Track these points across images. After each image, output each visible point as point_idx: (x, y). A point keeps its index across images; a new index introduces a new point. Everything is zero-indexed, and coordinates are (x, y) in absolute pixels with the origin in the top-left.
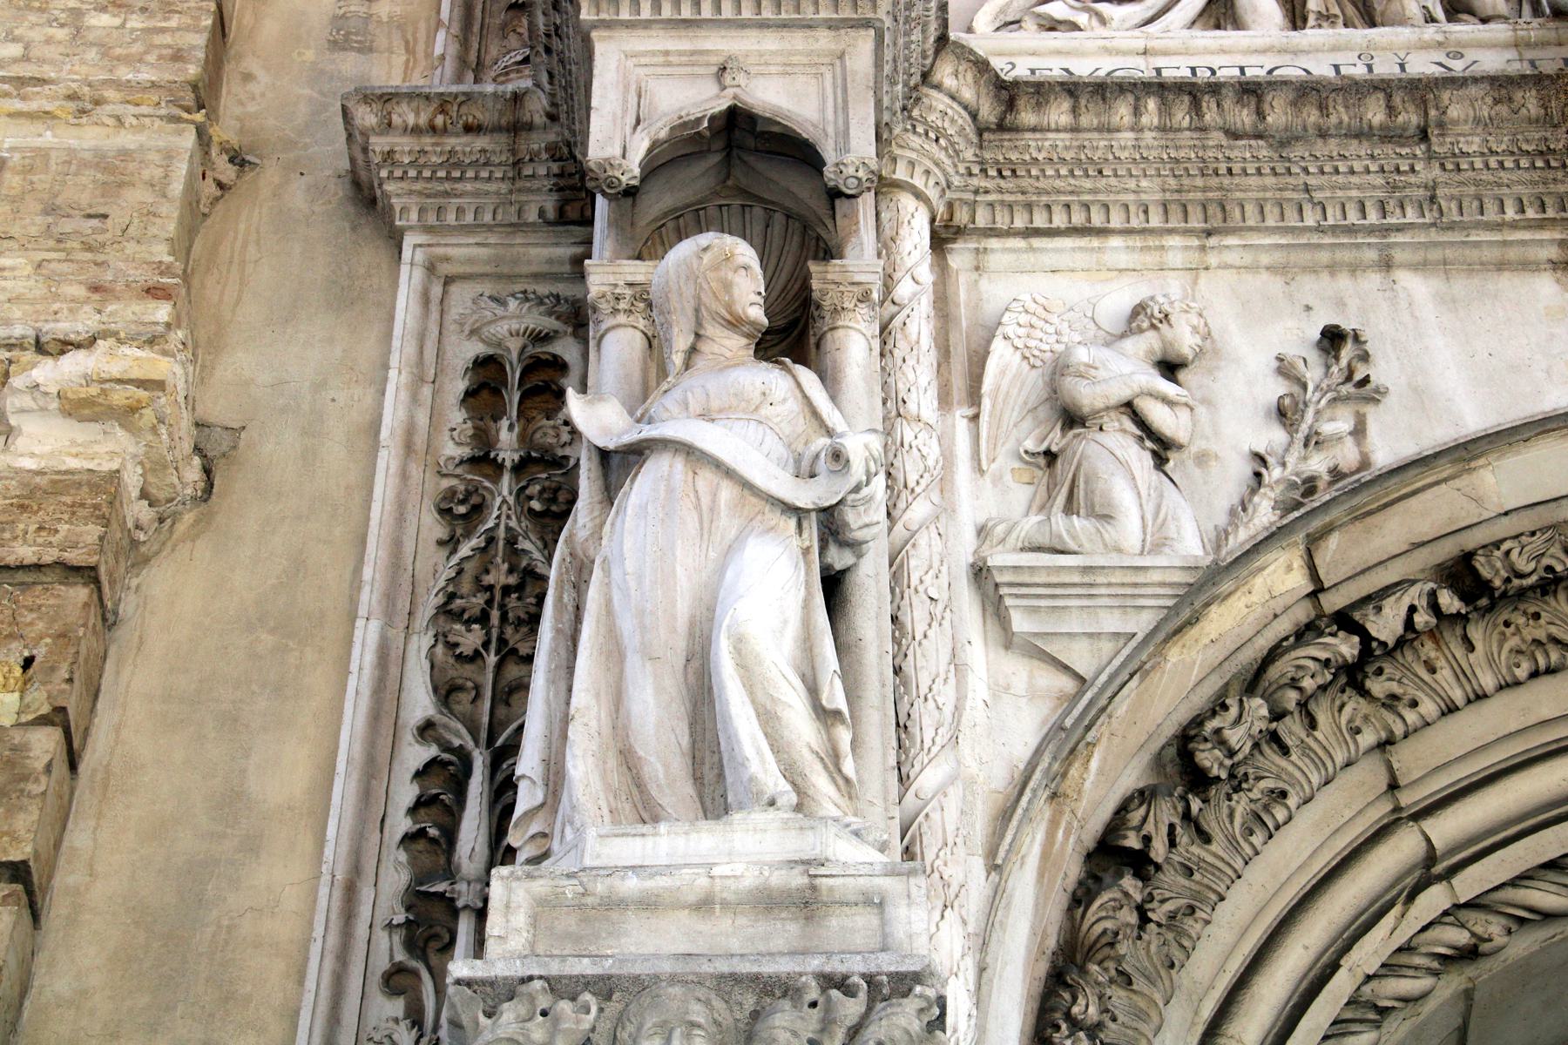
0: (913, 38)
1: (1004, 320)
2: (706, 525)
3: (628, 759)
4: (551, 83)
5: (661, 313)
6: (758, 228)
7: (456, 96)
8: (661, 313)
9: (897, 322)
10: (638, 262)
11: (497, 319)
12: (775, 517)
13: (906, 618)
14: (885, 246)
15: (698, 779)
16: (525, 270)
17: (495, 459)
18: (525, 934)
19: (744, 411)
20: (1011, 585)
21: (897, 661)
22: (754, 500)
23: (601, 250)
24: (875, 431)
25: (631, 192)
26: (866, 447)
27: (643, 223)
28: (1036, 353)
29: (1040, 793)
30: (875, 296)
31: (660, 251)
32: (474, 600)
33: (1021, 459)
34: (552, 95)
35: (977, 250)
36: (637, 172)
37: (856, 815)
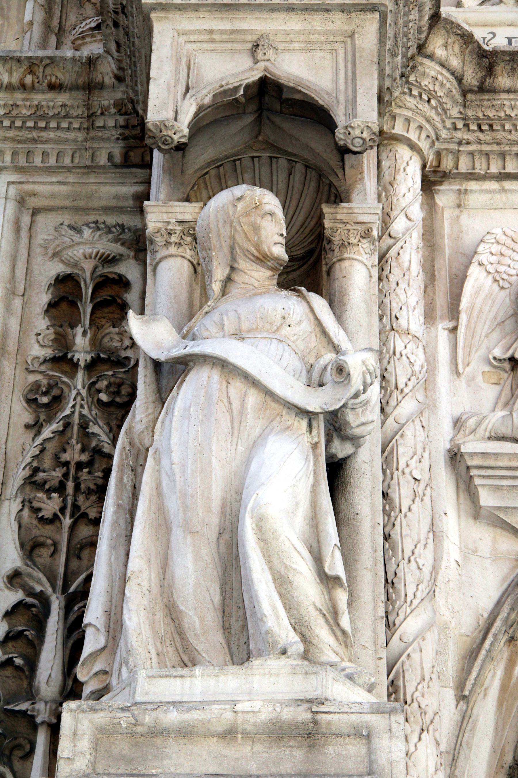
0: (411, 17)
1: (480, 249)
2: (236, 424)
3: (172, 613)
4: (118, 51)
5: (204, 249)
6: (282, 176)
7: (42, 60)
8: (204, 249)
9: (392, 252)
10: (186, 204)
11: (74, 244)
12: (290, 419)
13: (394, 495)
14: (385, 189)
15: (226, 629)
16: (96, 204)
17: (72, 359)
18: (88, 757)
19: (268, 331)
20: (480, 467)
21: (387, 530)
22: (274, 405)
23: (158, 192)
24: (371, 349)
25: (181, 148)
26: (364, 362)
27: (191, 171)
28: (505, 276)
29: (500, 637)
30: (375, 233)
31: (204, 194)
32: (54, 473)
33: (490, 364)
34: (119, 61)
35: (459, 190)
36: (186, 131)
37: (350, 661)
